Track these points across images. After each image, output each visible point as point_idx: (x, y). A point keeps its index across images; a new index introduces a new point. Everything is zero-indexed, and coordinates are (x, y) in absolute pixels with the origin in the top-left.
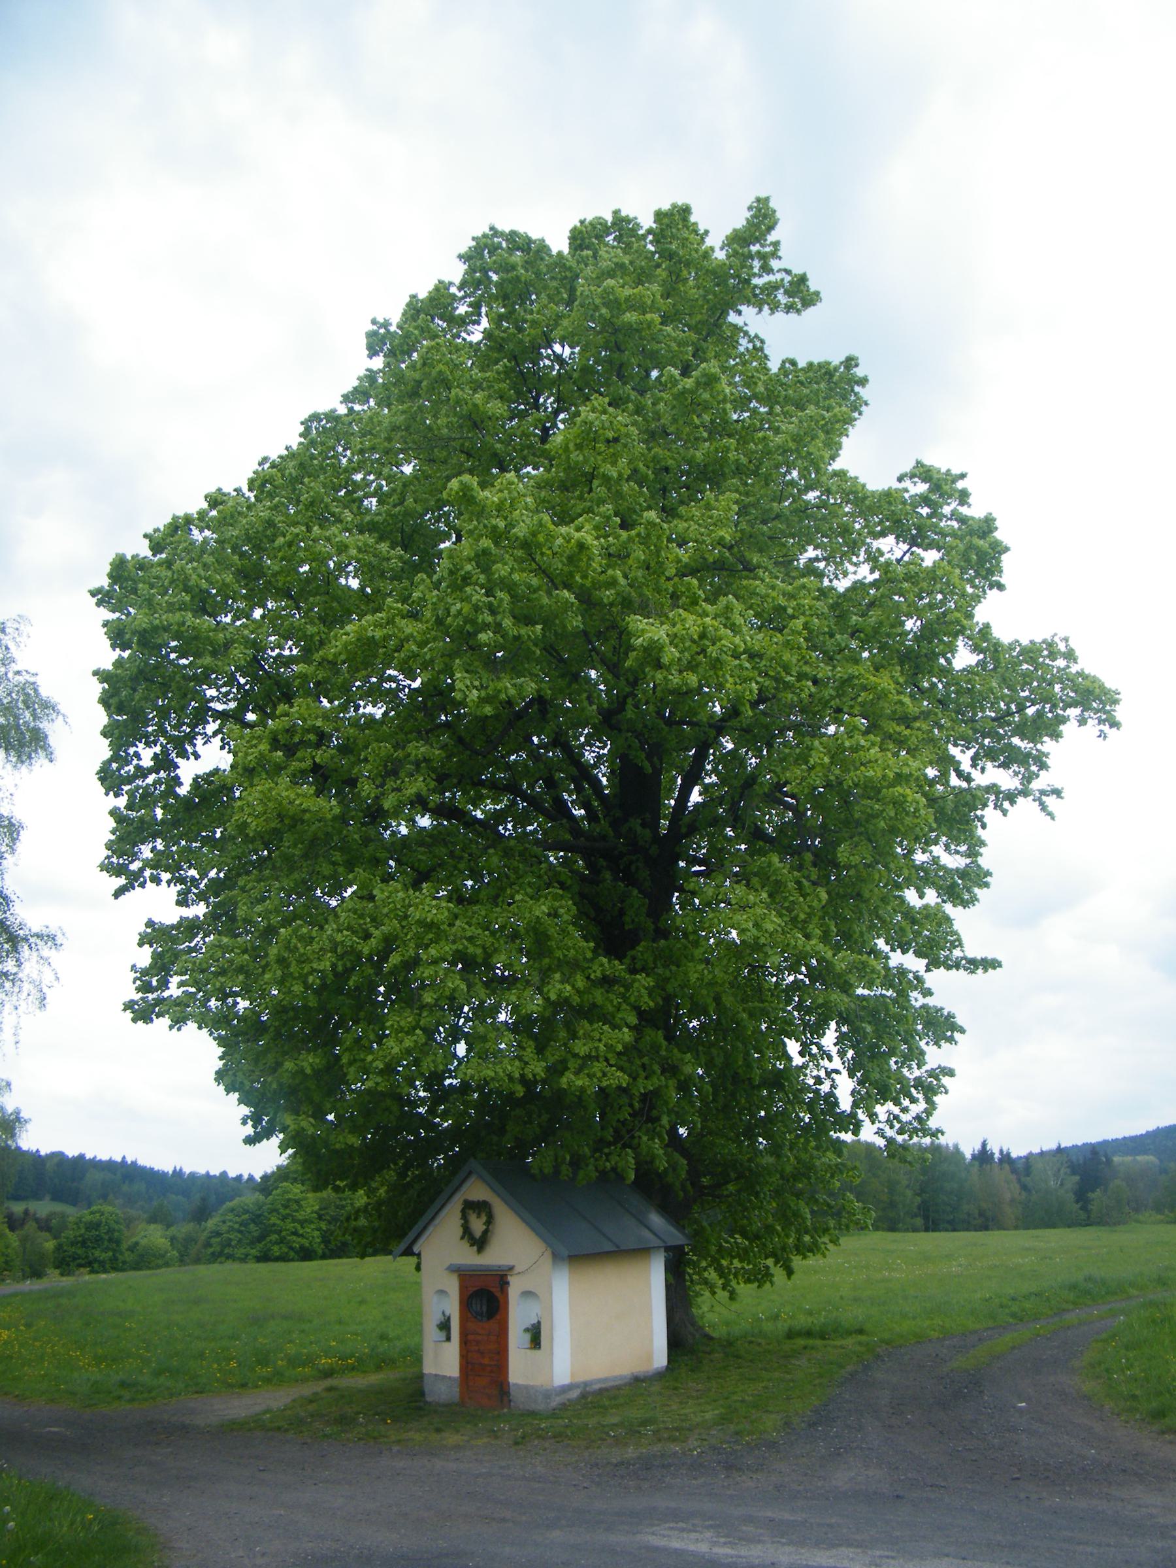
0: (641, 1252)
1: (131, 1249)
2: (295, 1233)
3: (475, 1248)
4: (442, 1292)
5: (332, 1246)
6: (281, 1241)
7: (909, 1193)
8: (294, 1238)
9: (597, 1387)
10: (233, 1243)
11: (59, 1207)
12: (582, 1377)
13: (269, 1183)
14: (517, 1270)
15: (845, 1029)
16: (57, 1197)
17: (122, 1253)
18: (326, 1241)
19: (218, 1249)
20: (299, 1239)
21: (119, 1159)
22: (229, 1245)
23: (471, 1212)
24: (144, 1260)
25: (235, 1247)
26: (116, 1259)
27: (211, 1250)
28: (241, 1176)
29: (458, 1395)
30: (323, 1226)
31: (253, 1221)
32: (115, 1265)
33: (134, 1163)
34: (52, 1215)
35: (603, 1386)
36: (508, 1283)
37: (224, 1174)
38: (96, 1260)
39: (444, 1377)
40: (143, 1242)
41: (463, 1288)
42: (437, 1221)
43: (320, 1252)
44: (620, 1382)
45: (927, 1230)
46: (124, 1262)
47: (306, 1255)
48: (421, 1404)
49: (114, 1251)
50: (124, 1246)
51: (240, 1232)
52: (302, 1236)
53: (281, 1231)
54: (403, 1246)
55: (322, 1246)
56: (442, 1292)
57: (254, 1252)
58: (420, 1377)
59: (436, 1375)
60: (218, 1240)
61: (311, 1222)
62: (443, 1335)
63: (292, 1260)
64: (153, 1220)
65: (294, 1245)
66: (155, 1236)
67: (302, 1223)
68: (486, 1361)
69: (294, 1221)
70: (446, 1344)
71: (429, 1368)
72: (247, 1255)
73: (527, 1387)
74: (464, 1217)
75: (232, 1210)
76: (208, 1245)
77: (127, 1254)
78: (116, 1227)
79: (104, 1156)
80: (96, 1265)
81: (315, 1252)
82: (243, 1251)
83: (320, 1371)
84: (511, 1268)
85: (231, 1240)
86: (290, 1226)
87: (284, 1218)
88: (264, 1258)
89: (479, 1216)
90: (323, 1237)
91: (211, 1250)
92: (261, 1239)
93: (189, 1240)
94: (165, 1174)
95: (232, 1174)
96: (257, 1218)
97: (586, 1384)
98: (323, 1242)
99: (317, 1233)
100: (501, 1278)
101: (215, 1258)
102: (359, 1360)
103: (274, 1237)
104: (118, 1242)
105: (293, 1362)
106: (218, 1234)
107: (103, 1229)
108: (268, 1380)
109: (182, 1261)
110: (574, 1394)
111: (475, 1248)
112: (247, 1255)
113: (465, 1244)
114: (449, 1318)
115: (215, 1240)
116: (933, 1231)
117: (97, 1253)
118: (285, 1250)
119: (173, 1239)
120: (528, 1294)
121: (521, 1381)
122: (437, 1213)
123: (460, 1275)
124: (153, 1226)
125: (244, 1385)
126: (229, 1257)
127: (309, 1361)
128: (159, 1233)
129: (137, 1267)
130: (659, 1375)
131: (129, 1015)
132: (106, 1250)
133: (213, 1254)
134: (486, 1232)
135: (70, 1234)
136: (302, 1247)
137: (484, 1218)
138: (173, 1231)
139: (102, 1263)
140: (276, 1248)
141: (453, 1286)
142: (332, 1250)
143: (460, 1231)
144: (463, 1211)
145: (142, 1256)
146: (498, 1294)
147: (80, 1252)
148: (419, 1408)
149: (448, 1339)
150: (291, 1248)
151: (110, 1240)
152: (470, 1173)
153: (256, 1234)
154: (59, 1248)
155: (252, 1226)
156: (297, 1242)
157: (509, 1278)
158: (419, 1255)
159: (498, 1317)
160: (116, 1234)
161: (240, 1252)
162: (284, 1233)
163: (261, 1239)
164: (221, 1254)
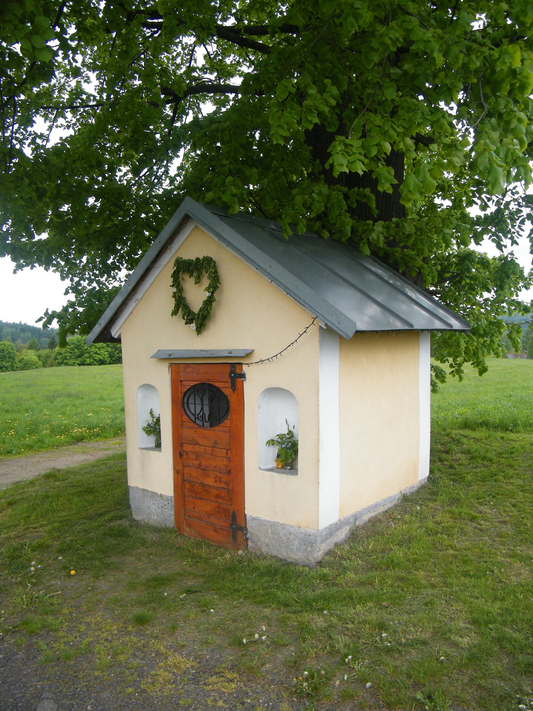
1: (20, 361)
2: (96, 353)
3: (193, 326)
4: (148, 387)
5: (114, 359)
6: (90, 357)
8: (96, 355)
9: (366, 518)
12: (350, 511)
14: (256, 358)
17: (16, 363)
18: (111, 357)
19: (61, 360)
20: (98, 356)
21: (18, 323)
22: (66, 359)
23: (186, 277)
24: (26, 366)
26: (13, 366)
27: (58, 361)
29: (172, 518)
31: (76, 347)
33: (25, 324)
35: (373, 514)
36: (243, 376)
38: (4, 366)
39: (154, 494)
40: (26, 358)
41: (176, 383)
42: (139, 295)
43: (108, 362)
44: (389, 505)
46: (17, 367)
47: (102, 362)
48: (125, 523)
49: (12, 362)
50: (17, 360)
51: (71, 353)
53: (90, 352)
55: (109, 359)
56: (148, 387)
57: (78, 362)
58: (126, 490)
59: (144, 490)
60: (61, 356)
61: (104, 348)
62: (151, 441)
63: (95, 365)
64: (31, 347)
65: (96, 358)
66: (31, 355)
68: (210, 481)
69: (95, 348)
70: (155, 454)
72: (74, 363)
73: (273, 525)
74: (177, 282)
76: (56, 359)
77: (18, 363)
78: (12, 351)
79: (11, 321)
80: (4, 369)
81: (106, 361)
82: (72, 361)
83: (73, 437)
84: (249, 354)
85: (66, 356)
88: (82, 364)
89: (198, 281)
91: (58, 361)
92: (80, 356)
93: (47, 357)
97: (356, 517)
98: (109, 357)
99: (107, 353)
101: (59, 364)
102: (103, 429)
104: (13, 359)
105: (54, 431)
107: (6, 352)
108: (30, 447)
109: (44, 366)
110: (342, 534)
111: (193, 326)
112: (74, 363)
113: (179, 322)
114: (158, 420)
115: (58, 357)
117: (4, 363)
119: (39, 357)
121: (264, 516)
123: (171, 365)
124: (30, 351)
125: (9, 452)
126: (66, 364)
127: (65, 430)
128: (33, 354)
129: (23, 368)
132: (8, 362)
133: (58, 363)
134: (209, 302)
136: (100, 360)
137: (206, 282)
138: (40, 352)
139: (7, 368)
140: (88, 360)
142: (114, 361)
143: (171, 304)
144: (176, 276)
145: (25, 364)
146: (227, 391)
148: (122, 533)
149: (158, 445)
150: (95, 360)
151: (10, 357)
152: (186, 219)
153: (78, 354)
155: (76, 350)
156: (97, 357)
157: (245, 368)
158: (119, 340)
159: (227, 422)
160: (12, 354)
161: (71, 362)
162: (91, 353)
163: (80, 356)
164: (62, 363)
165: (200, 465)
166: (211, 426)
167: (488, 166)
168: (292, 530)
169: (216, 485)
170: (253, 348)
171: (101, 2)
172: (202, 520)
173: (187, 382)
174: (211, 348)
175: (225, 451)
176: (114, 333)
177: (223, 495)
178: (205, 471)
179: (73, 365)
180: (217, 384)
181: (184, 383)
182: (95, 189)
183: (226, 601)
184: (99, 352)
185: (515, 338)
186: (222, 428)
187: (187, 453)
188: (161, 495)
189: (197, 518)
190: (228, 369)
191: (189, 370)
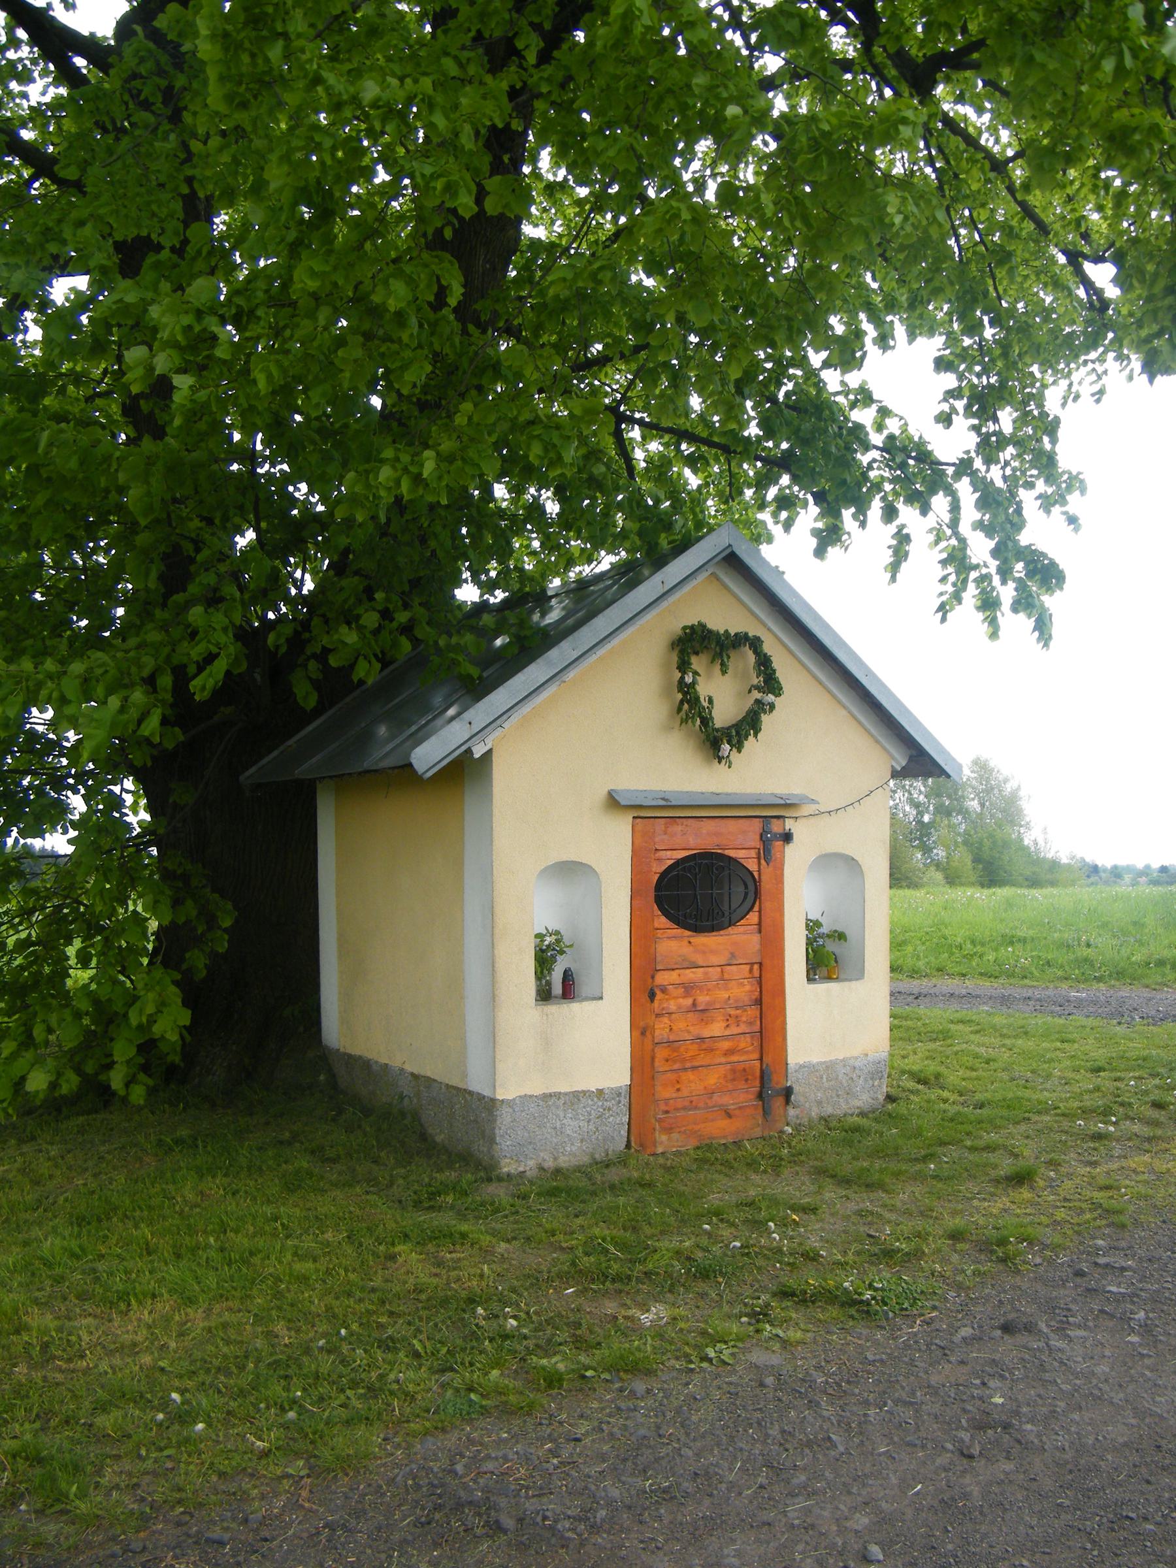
73: (829, 1066)
165: (694, 1004)
167: (7, 139)
168: (857, 1064)
169: (727, 1033)
170: (605, 792)
171: (999, 413)
172: (696, 1108)
174: (729, 790)
175: (747, 967)
177: (742, 1045)
178: (702, 1013)
180: (732, 853)
181: (662, 854)
182: (370, 408)
183: (716, 1249)
186: (741, 929)
187: (664, 990)
188: (600, 1092)
189: (684, 1108)
190: (757, 825)
191: (678, 828)
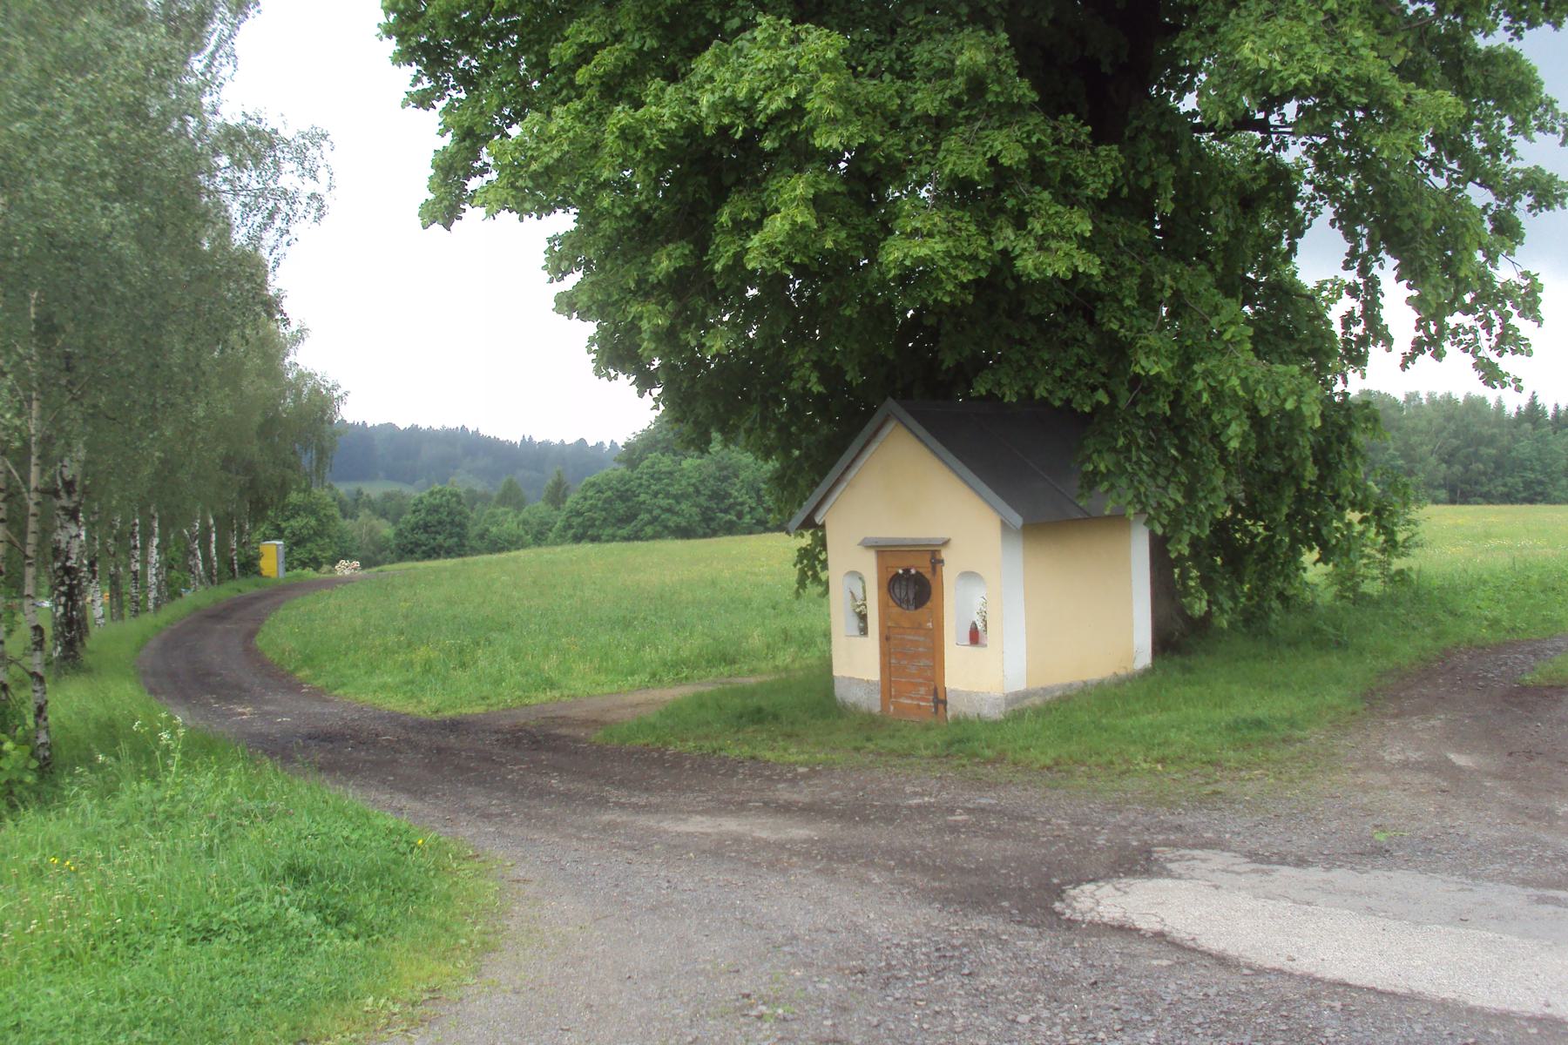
0: (1118, 520)
2: (669, 510)
7: (1433, 460)
10: (597, 523)
11: (393, 487)
13: (633, 454)
15: (1478, 181)
16: (391, 476)
20: (675, 518)
22: (592, 526)
25: (600, 527)
26: (463, 545)
28: (602, 443)
30: (702, 500)
32: (458, 550)
34: (388, 497)
37: (582, 441)
41: (882, 568)
43: (700, 531)
45: (1453, 502)
51: (605, 510)
52: (676, 513)
54: (800, 516)
59: (850, 678)
66: (509, 523)
67: (678, 498)
69: (668, 495)
71: (839, 671)
73: (968, 694)
75: (593, 485)
84: (946, 543)
85: (594, 520)
86: (665, 503)
87: (656, 495)
90: (703, 513)
94: (512, 446)
95: (591, 443)
96: (624, 496)
100: (933, 554)
101: (578, 539)
103: (645, 517)
104: (462, 526)
106: (579, 514)
116: (1462, 503)
118: (659, 528)
120: (969, 575)
121: (961, 687)
122: (854, 460)
126: (594, 539)
130: (1146, 674)
131: (437, 228)
132: (451, 535)
135: (409, 517)
141: (869, 566)
146: (928, 576)
147: (424, 537)
149: (864, 631)
151: (452, 523)
154: (399, 534)
156: (673, 521)
158: (823, 527)
166: (916, 608)
173: (1236, 868)
176: (818, 519)
179: (613, 538)
184: (677, 508)
185: (56, 638)
190: (928, 557)
